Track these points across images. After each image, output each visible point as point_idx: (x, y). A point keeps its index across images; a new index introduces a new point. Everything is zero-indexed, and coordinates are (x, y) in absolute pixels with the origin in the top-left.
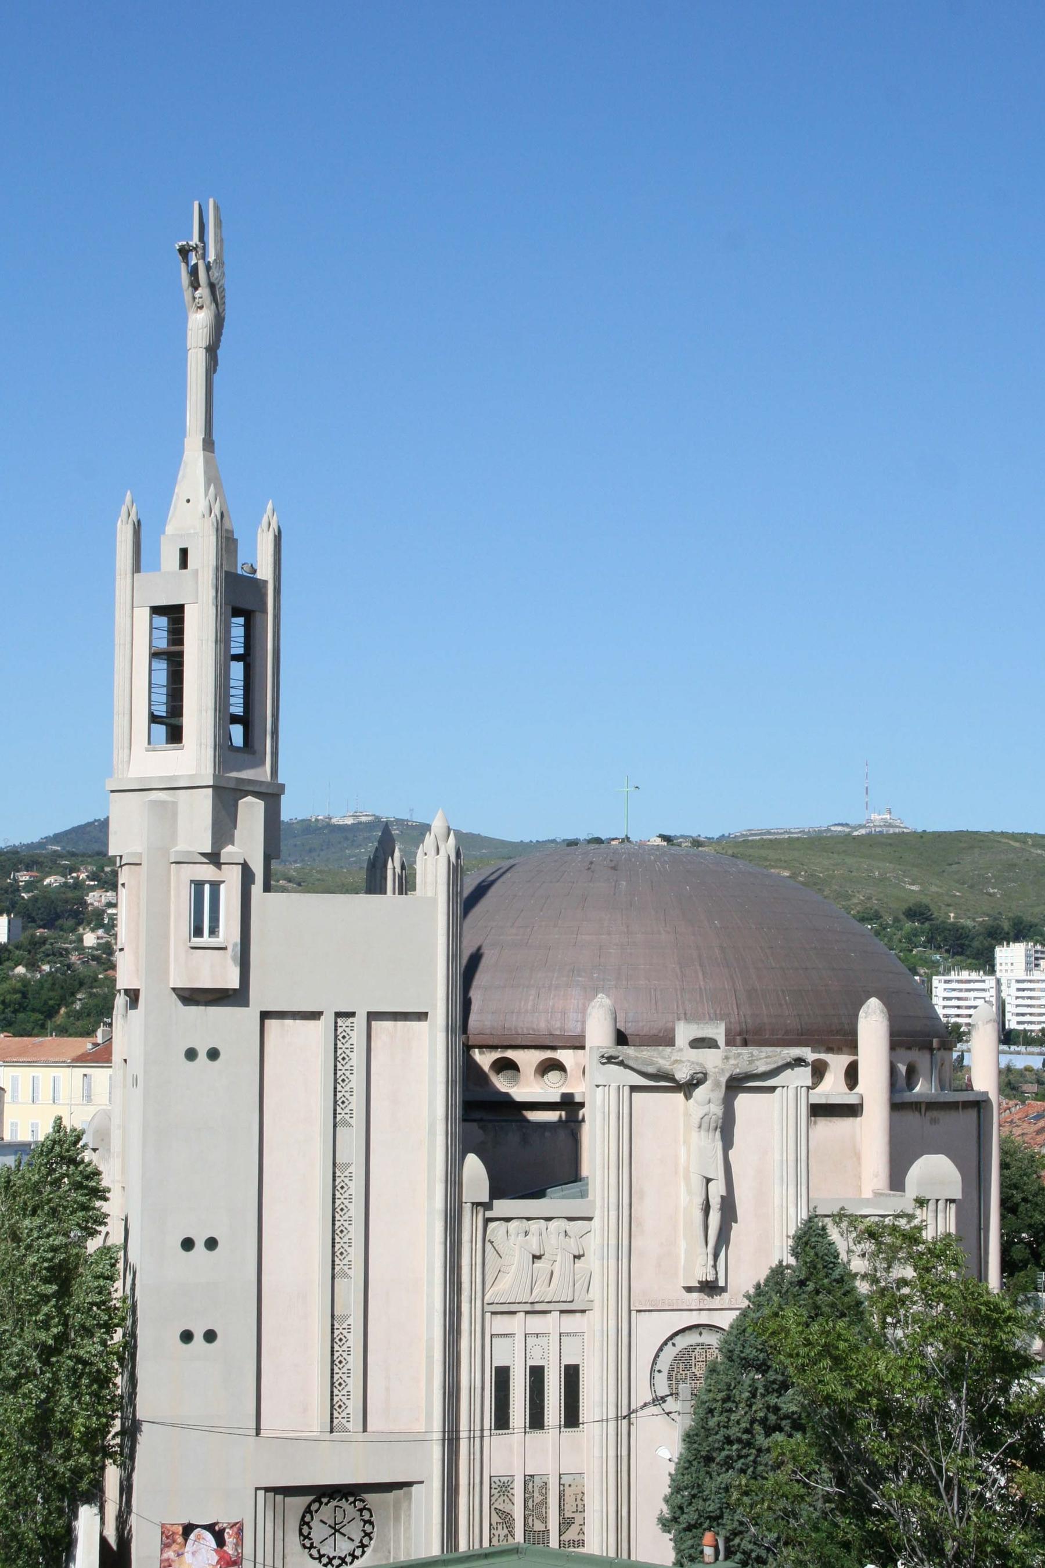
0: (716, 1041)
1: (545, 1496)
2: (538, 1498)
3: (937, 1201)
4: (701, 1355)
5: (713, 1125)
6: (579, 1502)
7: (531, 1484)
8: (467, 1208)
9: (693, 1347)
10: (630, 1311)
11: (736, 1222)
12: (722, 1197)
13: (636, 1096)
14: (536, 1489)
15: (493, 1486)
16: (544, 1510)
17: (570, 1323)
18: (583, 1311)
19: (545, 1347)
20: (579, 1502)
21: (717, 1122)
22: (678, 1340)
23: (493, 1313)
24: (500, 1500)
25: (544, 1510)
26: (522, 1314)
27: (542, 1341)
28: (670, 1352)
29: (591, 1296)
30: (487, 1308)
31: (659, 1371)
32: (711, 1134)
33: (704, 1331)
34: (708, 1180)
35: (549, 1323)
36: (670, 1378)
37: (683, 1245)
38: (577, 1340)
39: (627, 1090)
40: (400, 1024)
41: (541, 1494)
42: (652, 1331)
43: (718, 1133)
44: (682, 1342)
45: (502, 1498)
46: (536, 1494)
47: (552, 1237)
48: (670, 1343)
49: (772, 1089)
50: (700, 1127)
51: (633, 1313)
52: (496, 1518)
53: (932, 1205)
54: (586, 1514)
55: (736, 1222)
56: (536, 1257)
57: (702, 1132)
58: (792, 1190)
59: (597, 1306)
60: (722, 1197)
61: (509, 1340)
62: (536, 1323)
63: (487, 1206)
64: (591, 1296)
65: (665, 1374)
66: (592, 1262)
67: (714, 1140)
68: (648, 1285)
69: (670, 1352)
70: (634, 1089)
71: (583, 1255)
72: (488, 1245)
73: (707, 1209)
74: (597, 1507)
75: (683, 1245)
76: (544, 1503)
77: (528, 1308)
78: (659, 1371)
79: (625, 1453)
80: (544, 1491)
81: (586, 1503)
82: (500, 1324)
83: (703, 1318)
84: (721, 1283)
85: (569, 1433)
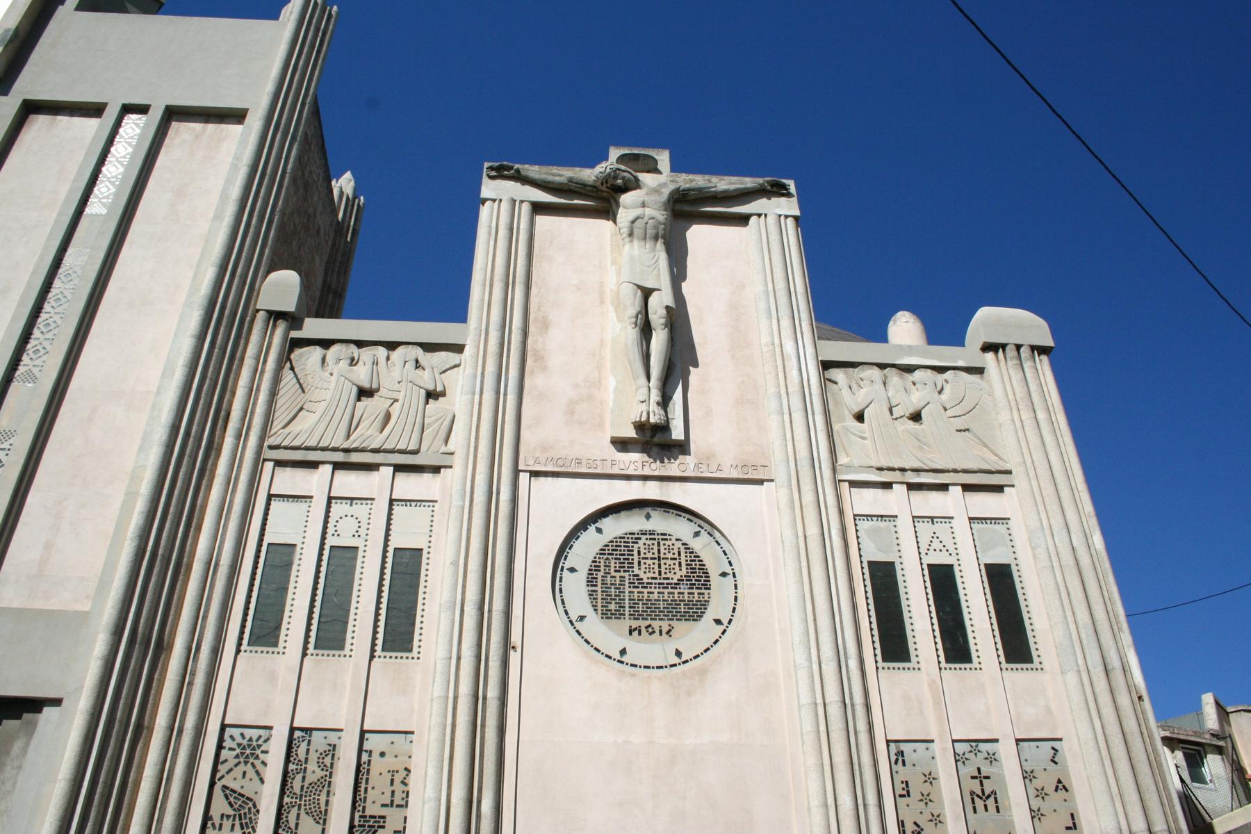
0: (656, 162)
1: (329, 771)
2: (314, 772)
3: (1018, 347)
4: (649, 549)
5: (650, 232)
6: (398, 787)
7: (304, 746)
8: (261, 316)
9: (635, 537)
10: (516, 472)
11: (696, 365)
12: (667, 308)
13: (541, 220)
14: (313, 757)
15: (228, 743)
16: (323, 798)
17: (408, 485)
18: (436, 470)
19: (364, 521)
20: (398, 787)
21: (656, 227)
22: (607, 523)
23: (279, 463)
24: (238, 772)
25: (323, 798)
26: (329, 468)
27: (360, 510)
28: (589, 544)
29: (451, 446)
30: (268, 454)
31: (572, 570)
32: (649, 245)
33: (653, 513)
34: (647, 293)
35: (376, 484)
36: (591, 581)
37: (611, 383)
38: (423, 512)
39: (526, 208)
40: (211, 127)
41: (322, 766)
42: (553, 508)
43: (660, 241)
44: (614, 527)
45: (242, 768)
46: (312, 766)
47: (397, 374)
48: (592, 528)
49: (743, 220)
50: (631, 235)
51: (524, 478)
52: (220, 806)
53: (1011, 351)
54: (410, 812)
55: (696, 365)
56: (364, 393)
57: (636, 242)
58: (786, 323)
59: (457, 461)
60: (667, 308)
61: (302, 506)
62: (349, 483)
63: (294, 320)
64: (451, 446)
65: (582, 575)
66: (458, 401)
67: (654, 250)
68: (546, 435)
69: (589, 544)
70: (538, 208)
71: (443, 394)
72: (287, 375)
73: (646, 330)
74: (430, 793)
75: (611, 383)
76: (326, 783)
77: (339, 457)
78: (572, 570)
79: (493, 692)
80: (328, 761)
81: (411, 788)
82: (288, 480)
83: (652, 491)
84: (677, 434)
85: (386, 664)
